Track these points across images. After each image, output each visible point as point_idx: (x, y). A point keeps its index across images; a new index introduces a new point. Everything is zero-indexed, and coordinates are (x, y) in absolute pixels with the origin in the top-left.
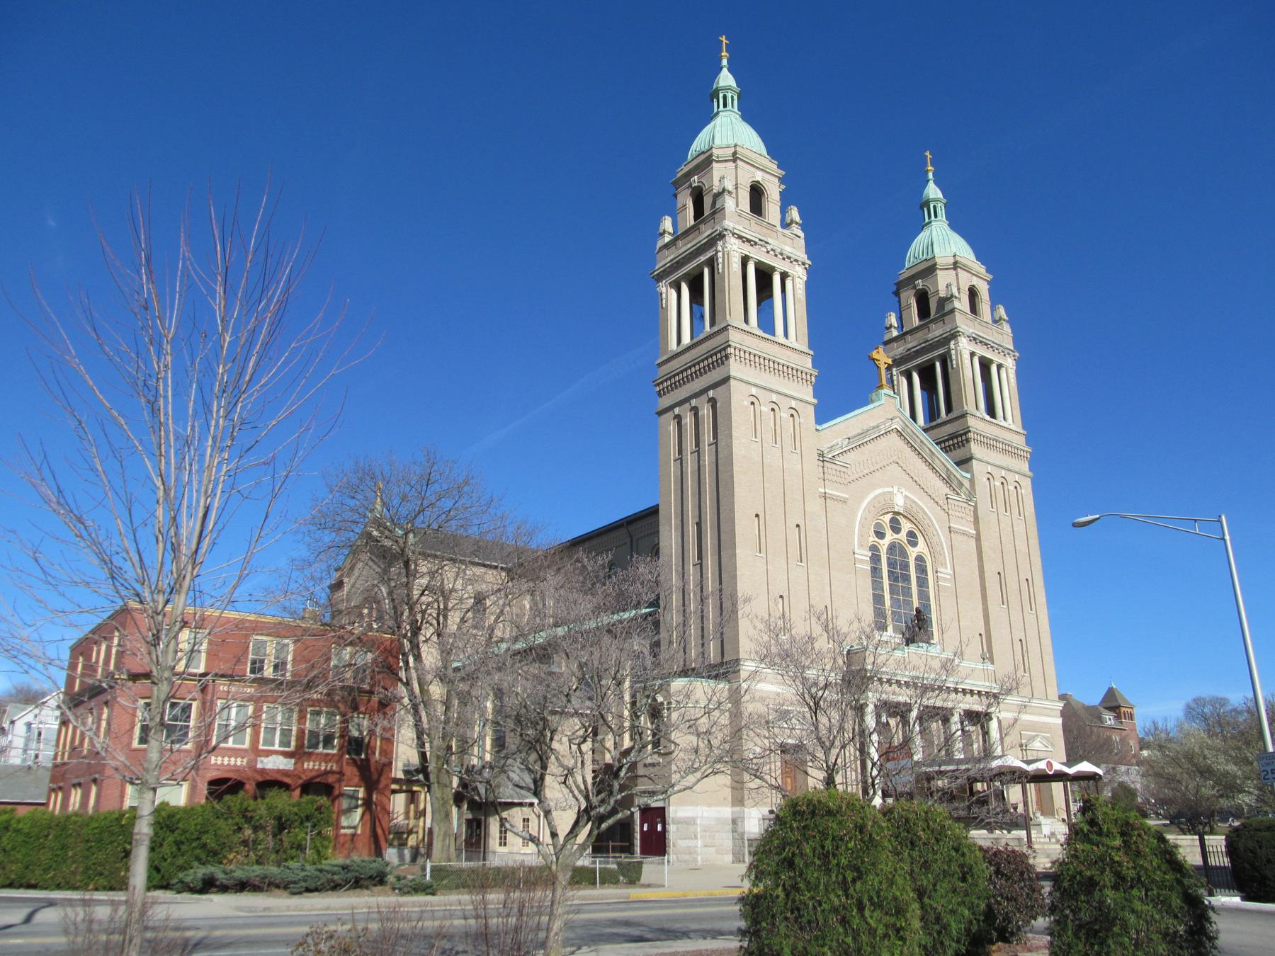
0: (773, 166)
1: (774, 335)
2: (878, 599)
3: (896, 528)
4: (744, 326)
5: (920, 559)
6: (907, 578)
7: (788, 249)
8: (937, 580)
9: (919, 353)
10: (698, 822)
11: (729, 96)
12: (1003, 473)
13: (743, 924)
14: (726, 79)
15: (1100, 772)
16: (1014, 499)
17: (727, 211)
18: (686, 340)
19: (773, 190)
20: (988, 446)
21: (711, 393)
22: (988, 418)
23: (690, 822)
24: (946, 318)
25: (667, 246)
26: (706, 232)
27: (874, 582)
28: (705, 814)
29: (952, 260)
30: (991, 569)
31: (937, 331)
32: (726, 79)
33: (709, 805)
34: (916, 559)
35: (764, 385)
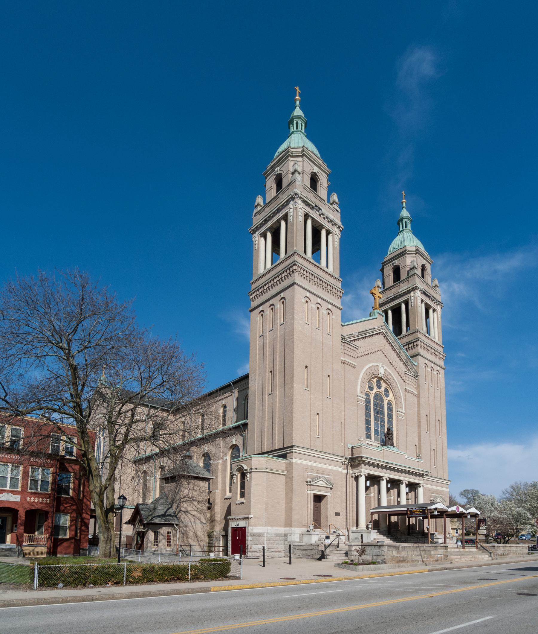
0: (324, 166)
1: (320, 263)
2: (368, 422)
3: (379, 387)
4: (303, 255)
5: (389, 404)
6: (383, 413)
7: (331, 214)
8: (397, 415)
9: (392, 300)
10: (265, 535)
11: (300, 122)
12: (432, 365)
13: (152, 461)
14: (298, 112)
15: (479, 513)
16: (436, 379)
17: (297, 183)
18: (269, 266)
19: (323, 182)
20: (427, 350)
21: (282, 295)
22: (427, 335)
23: (259, 535)
24: (410, 279)
25: (259, 213)
26: (284, 198)
27: (366, 413)
28: (269, 531)
29: (414, 249)
30: (423, 413)
31: (403, 287)
32: (298, 112)
33: (272, 526)
34: (388, 404)
35: (314, 292)
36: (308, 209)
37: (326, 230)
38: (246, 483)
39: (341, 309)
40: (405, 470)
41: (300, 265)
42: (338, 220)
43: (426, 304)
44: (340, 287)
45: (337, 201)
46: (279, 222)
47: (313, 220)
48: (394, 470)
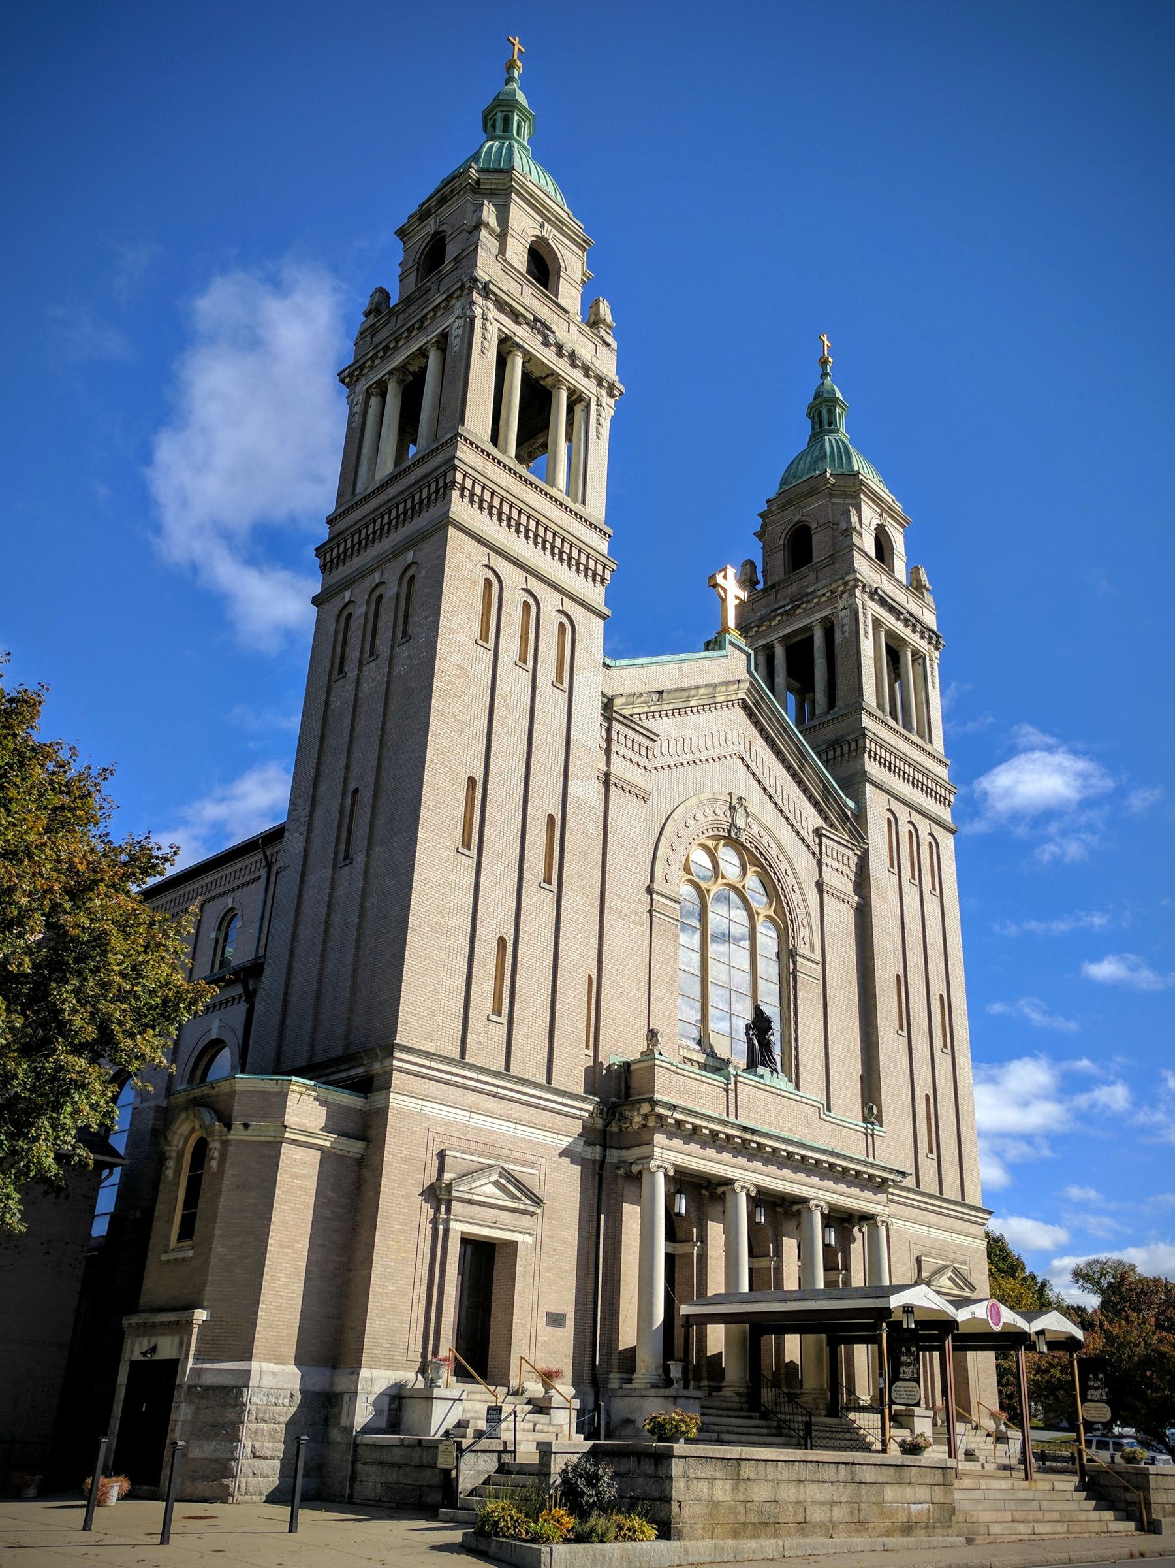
0: (576, 225)
1: (553, 485)
15: (1079, 1334)
36: (509, 325)
37: (569, 389)
38: (206, 1180)
39: (603, 617)
40: (818, 1162)
41: (469, 470)
42: (607, 363)
43: (890, 634)
44: (946, 779)
45: (609, 319)
46: (422, 353)
47: (528, 357)
48: (773, 1158)
